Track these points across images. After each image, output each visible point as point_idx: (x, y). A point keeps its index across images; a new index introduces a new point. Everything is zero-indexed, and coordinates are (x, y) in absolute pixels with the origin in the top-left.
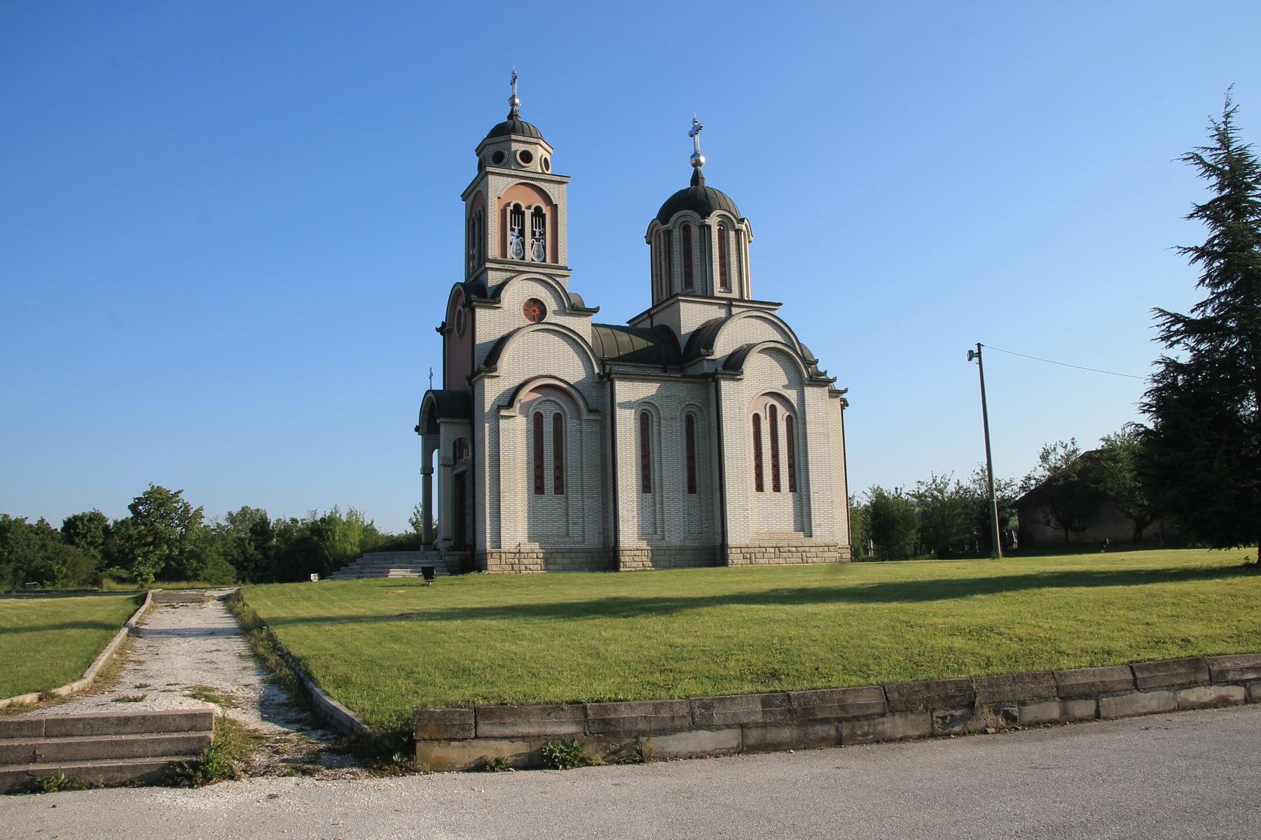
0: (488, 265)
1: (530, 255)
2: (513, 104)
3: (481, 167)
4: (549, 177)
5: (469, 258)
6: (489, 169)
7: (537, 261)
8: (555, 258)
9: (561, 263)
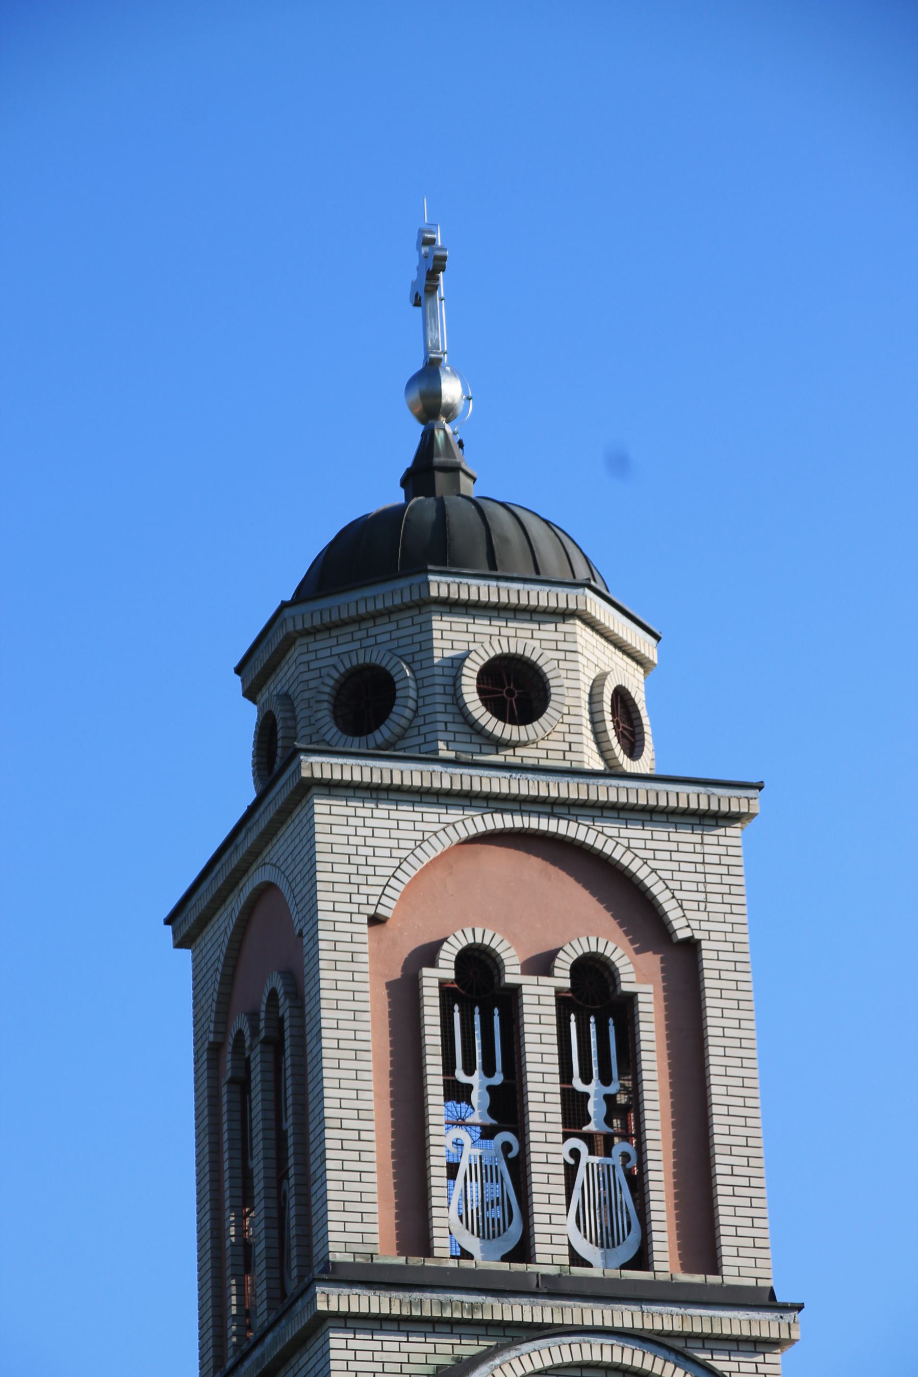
0: (330, 1299)
1: (558, 1230)
2: (431, 409)
3: (273, 754)
4: (642, 794)
5: (222, 1262)
6: (317, 766)
7: (600, 1265)
8: (702, 1240)
9: (736, 1269)
